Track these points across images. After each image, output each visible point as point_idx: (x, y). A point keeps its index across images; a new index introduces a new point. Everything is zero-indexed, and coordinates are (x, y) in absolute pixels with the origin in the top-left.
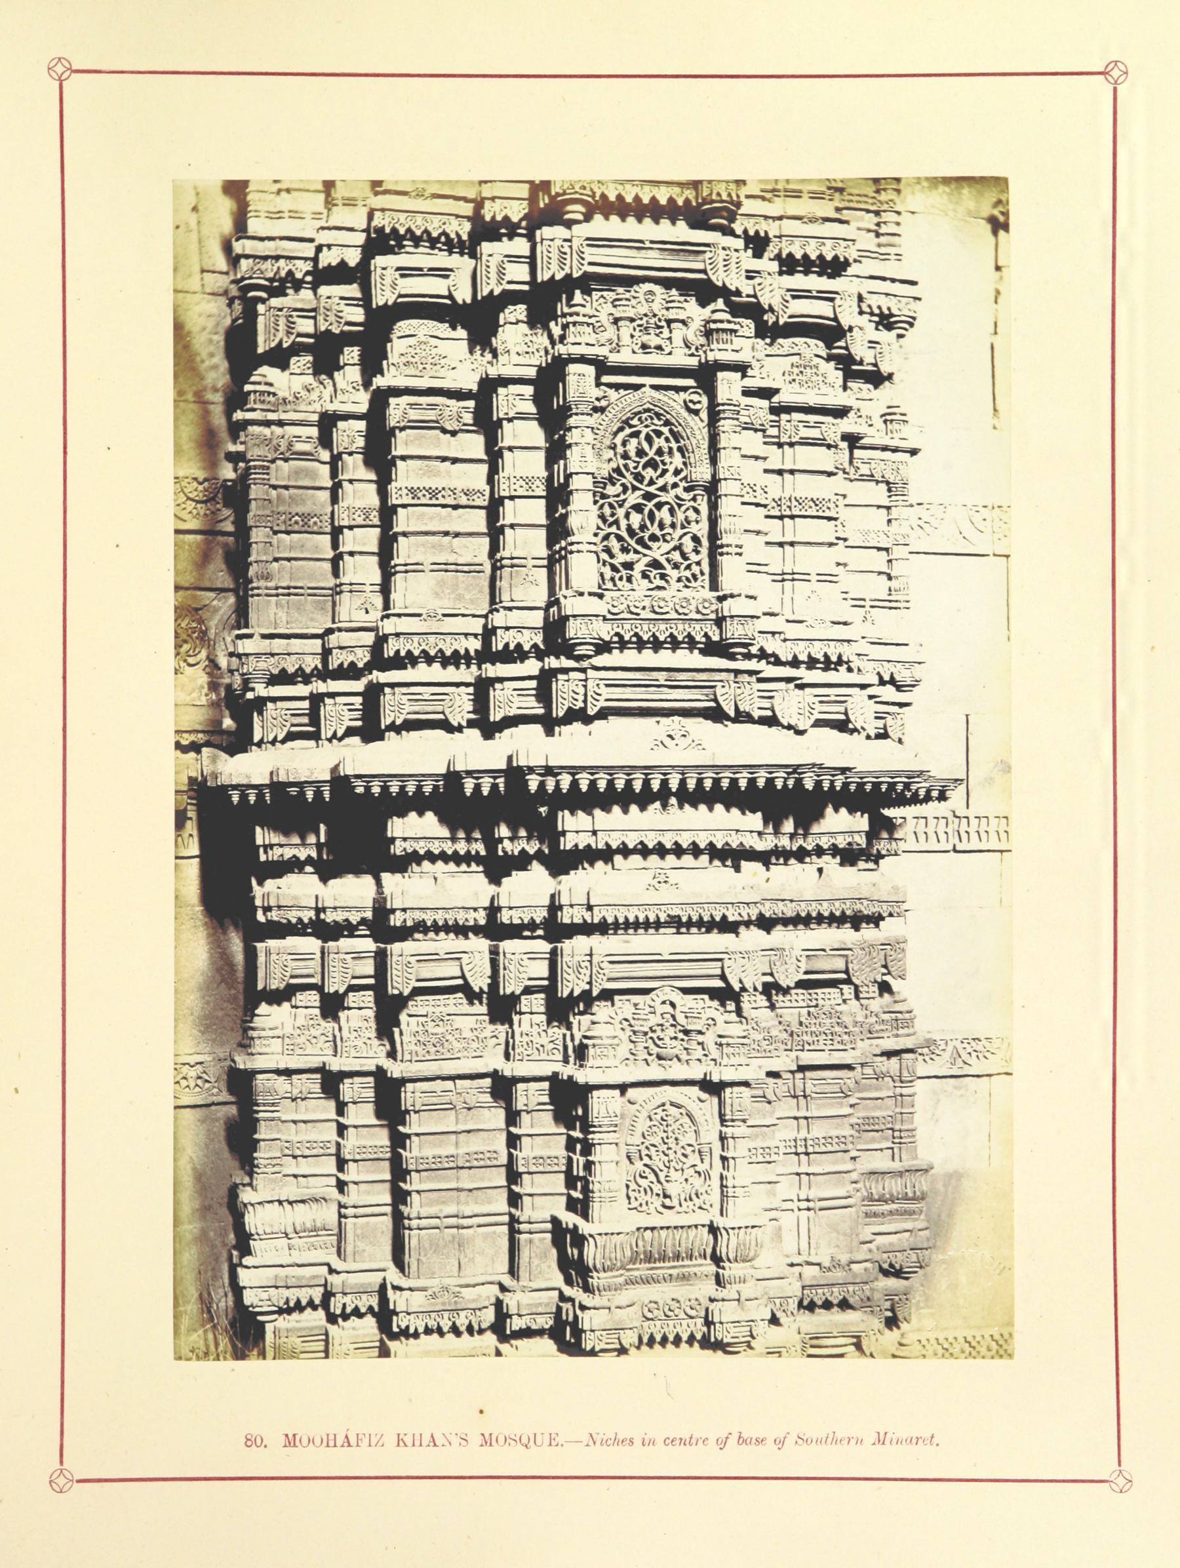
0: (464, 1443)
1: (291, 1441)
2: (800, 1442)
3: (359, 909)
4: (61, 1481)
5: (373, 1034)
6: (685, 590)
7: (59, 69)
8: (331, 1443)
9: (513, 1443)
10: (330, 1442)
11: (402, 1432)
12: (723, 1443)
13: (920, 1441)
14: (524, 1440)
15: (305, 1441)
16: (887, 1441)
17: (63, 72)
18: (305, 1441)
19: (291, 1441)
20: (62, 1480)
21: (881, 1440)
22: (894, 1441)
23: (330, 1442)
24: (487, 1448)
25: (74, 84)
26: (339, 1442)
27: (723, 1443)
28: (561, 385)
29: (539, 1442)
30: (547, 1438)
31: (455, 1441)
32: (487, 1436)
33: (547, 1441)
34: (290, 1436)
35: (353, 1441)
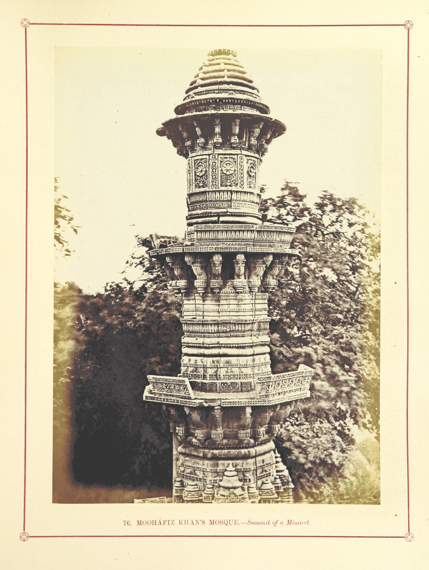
0: (203, 523)
1: (140, 523)
2: (249, 523)
3: (268, 342)
4: (24, 537)
5: (308, 389)
6: (349, 219)
7: (25, 23)
8: (154, 524)
9: (222, 523)
10: (154, 523)
11: (181, 519)
12: (275, 524)
13: (304, 523)
14: (226, 522)
15: (145, 523)
16: (292, 523)
17: (27, 25)
18: (145, 523)
19: (140, 523)
20: (25, 536)
21: (289, 522)
22: (294, 523)
23: (154, 523)
24: (212, 525)
25: (30, 29)
26: (157, 523)
27: (275, 524)
28: (245, 131)
29: (231, 523)
30: (234, 521)
31: (200, 523)
32: (212, 521)
33: (234, 523)
34: (139, 522)
35: (162, 523)
